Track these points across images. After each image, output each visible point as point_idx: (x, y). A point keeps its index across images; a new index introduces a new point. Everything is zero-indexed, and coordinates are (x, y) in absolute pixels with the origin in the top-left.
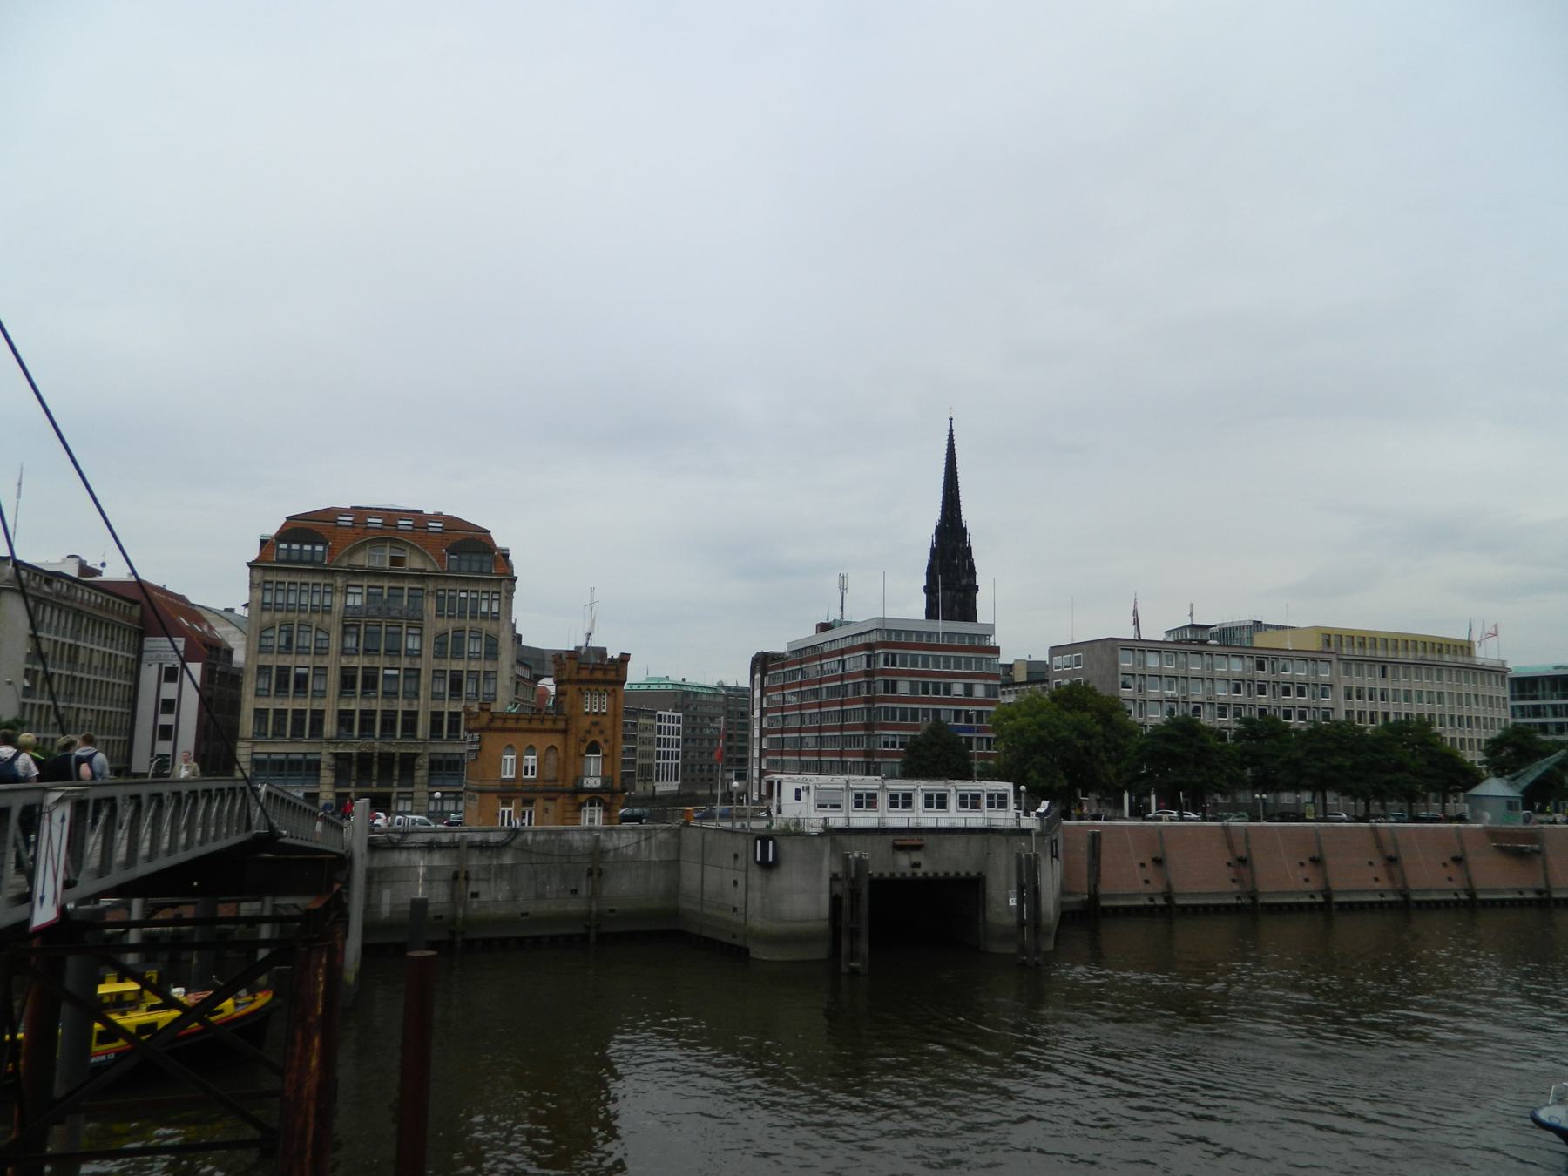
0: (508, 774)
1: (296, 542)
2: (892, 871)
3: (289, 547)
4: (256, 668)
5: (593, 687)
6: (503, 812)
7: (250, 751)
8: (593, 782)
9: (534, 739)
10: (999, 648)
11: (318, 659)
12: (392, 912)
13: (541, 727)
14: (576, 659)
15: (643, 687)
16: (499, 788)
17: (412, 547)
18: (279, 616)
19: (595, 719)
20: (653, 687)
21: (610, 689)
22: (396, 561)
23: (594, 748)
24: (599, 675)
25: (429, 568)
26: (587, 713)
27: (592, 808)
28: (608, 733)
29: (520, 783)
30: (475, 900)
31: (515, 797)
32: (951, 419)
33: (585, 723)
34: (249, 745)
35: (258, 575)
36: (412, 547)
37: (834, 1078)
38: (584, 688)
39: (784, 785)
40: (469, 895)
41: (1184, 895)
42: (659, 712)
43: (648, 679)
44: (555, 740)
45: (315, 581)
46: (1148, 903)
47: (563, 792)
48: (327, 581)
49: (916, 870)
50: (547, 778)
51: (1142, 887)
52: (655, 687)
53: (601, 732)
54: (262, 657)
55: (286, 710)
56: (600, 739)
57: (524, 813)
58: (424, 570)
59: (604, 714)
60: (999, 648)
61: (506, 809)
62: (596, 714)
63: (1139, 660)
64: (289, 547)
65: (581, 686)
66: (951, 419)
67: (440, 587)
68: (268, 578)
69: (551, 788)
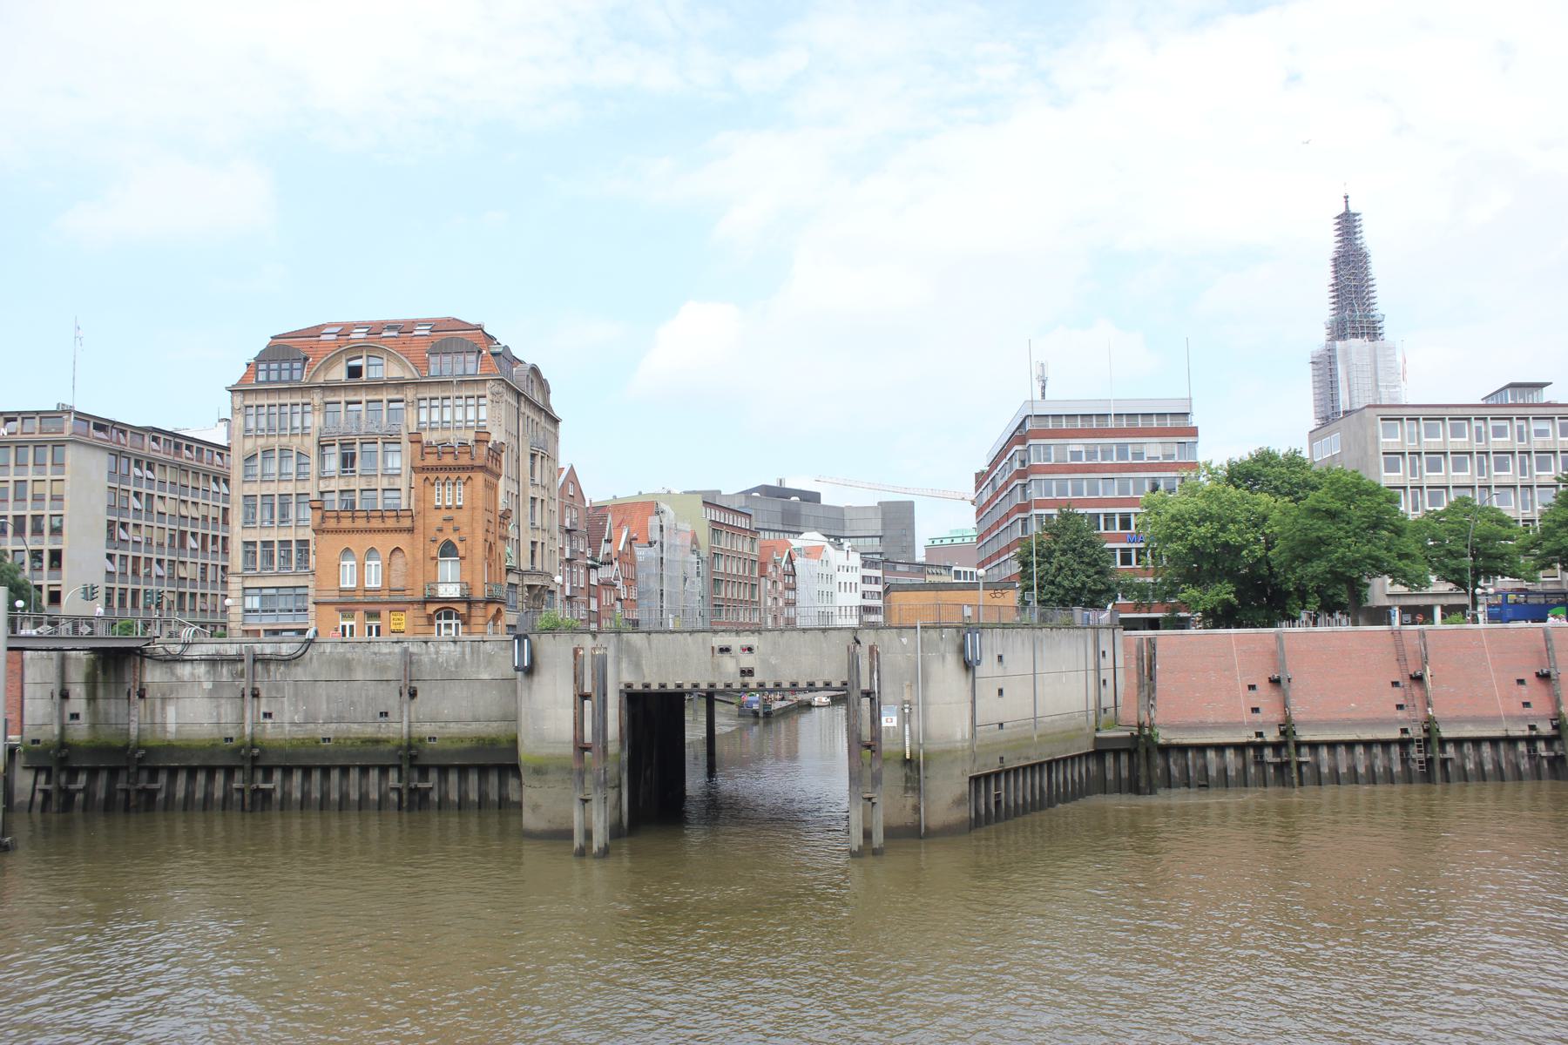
0: (348, 582)
1: (274, 361)
2: (712, 680)
3: (268, 367)
4: (241, 498)
5: (443, 476)
6: (344, 628)
7: (240, 587)
8: (449, 591)
9: (377, 541)
10: (1196, 428)
11: (299, 484)
12: (177, 731)
13: (382, 526)
14: (419, 442)
15: (945, 541)
16: (337, 599)
17: (389, 353)
18: (261, 441)
19: (448, 514)
20: (956, 541)
21: (464, 476)
22: (355, 372)
23: (448, 550)
24: (448, 460)
25: (408, 376)
26: (438, 508)
27: (448, 622)
28: (465, 530)
29: (361, 593)
30: (268, 721)
31: (357, 610)
32: (1346, 197)
33: (436, 519)
34: (240, 579)
35: (238, 399)
36: (389, 353)
37: (97, 904)
38: (432, 476)
39: (288, 530)
40: (262, 715)
41: (1308, 724)
42: (954, 568)
43: (951, 532)
44: (401, 540)
45: (293, 401)
46: (1254, 739)
47: (411, 603)
48: (306, 400)
49: (747, 679)
50: (393, 587)
51: (1247, 716)
52: (959, 541)
53: (456, 530)
54: (246, 486)
55: (273, 542)
56: (454, 538)
57: (370, 628)
58: (403, 378)
59: (459, 508)
60: (1196, 428)
61: (348, 623)
62: (448, 508)
63: (1410, 434)
64: (268, 367)
65: (429, 475)
66: (1346, 197)
67: (420, 396)
68: (248, 403)
69: (398, 599)
